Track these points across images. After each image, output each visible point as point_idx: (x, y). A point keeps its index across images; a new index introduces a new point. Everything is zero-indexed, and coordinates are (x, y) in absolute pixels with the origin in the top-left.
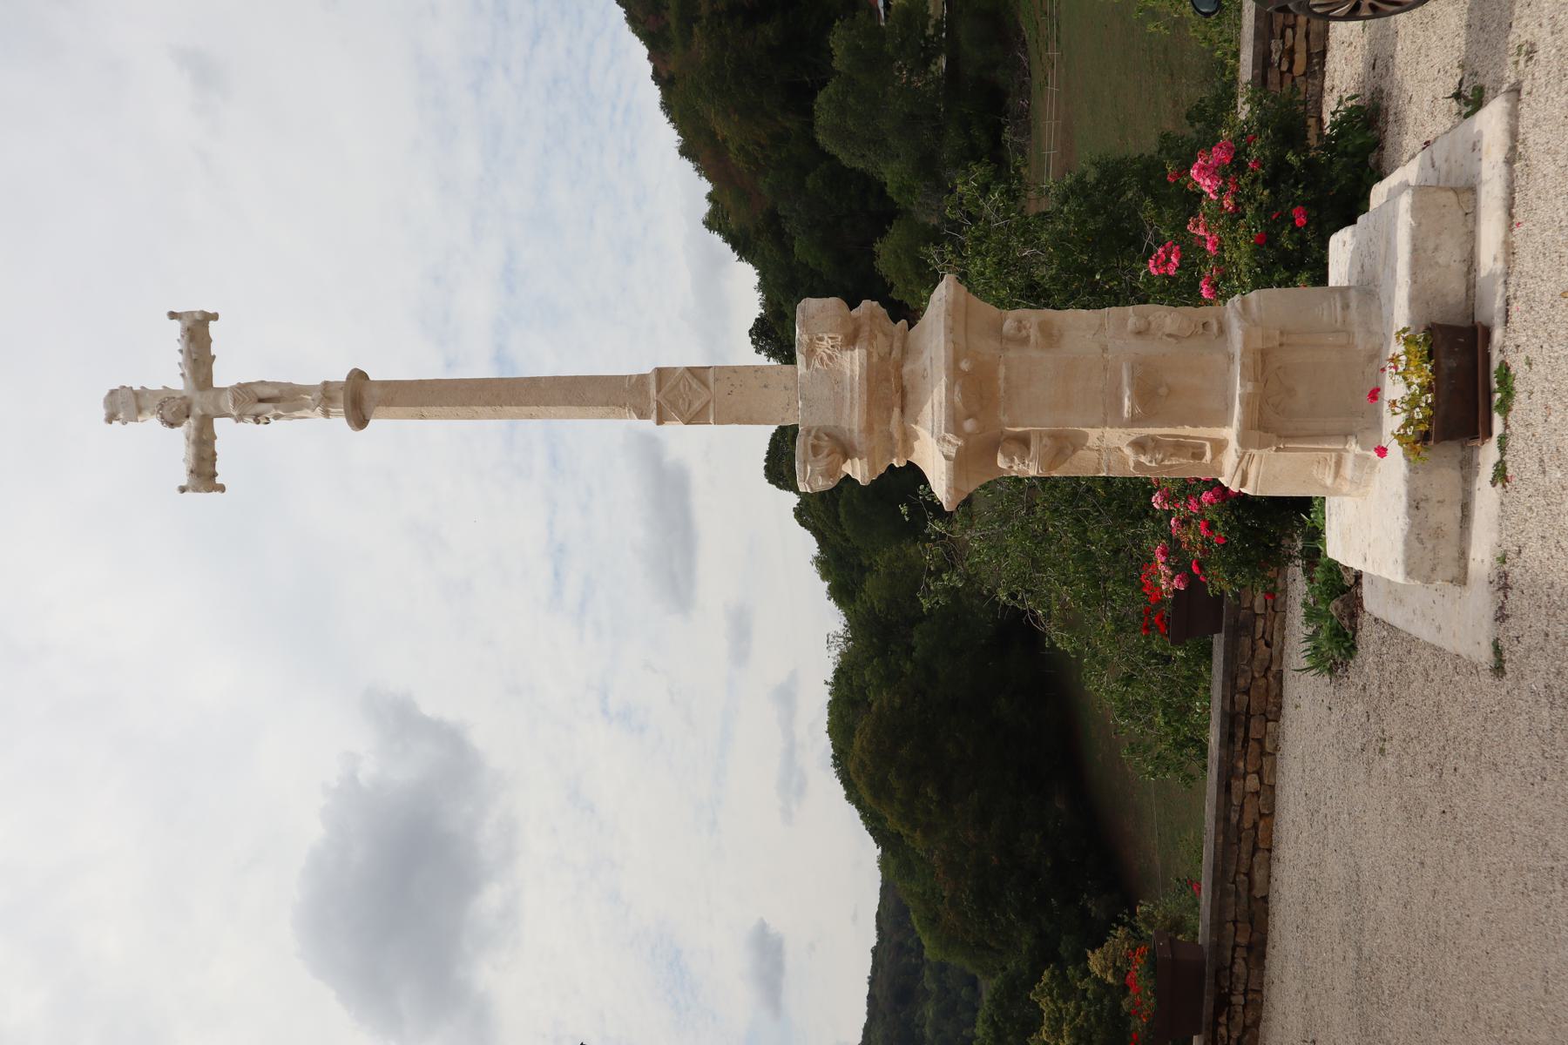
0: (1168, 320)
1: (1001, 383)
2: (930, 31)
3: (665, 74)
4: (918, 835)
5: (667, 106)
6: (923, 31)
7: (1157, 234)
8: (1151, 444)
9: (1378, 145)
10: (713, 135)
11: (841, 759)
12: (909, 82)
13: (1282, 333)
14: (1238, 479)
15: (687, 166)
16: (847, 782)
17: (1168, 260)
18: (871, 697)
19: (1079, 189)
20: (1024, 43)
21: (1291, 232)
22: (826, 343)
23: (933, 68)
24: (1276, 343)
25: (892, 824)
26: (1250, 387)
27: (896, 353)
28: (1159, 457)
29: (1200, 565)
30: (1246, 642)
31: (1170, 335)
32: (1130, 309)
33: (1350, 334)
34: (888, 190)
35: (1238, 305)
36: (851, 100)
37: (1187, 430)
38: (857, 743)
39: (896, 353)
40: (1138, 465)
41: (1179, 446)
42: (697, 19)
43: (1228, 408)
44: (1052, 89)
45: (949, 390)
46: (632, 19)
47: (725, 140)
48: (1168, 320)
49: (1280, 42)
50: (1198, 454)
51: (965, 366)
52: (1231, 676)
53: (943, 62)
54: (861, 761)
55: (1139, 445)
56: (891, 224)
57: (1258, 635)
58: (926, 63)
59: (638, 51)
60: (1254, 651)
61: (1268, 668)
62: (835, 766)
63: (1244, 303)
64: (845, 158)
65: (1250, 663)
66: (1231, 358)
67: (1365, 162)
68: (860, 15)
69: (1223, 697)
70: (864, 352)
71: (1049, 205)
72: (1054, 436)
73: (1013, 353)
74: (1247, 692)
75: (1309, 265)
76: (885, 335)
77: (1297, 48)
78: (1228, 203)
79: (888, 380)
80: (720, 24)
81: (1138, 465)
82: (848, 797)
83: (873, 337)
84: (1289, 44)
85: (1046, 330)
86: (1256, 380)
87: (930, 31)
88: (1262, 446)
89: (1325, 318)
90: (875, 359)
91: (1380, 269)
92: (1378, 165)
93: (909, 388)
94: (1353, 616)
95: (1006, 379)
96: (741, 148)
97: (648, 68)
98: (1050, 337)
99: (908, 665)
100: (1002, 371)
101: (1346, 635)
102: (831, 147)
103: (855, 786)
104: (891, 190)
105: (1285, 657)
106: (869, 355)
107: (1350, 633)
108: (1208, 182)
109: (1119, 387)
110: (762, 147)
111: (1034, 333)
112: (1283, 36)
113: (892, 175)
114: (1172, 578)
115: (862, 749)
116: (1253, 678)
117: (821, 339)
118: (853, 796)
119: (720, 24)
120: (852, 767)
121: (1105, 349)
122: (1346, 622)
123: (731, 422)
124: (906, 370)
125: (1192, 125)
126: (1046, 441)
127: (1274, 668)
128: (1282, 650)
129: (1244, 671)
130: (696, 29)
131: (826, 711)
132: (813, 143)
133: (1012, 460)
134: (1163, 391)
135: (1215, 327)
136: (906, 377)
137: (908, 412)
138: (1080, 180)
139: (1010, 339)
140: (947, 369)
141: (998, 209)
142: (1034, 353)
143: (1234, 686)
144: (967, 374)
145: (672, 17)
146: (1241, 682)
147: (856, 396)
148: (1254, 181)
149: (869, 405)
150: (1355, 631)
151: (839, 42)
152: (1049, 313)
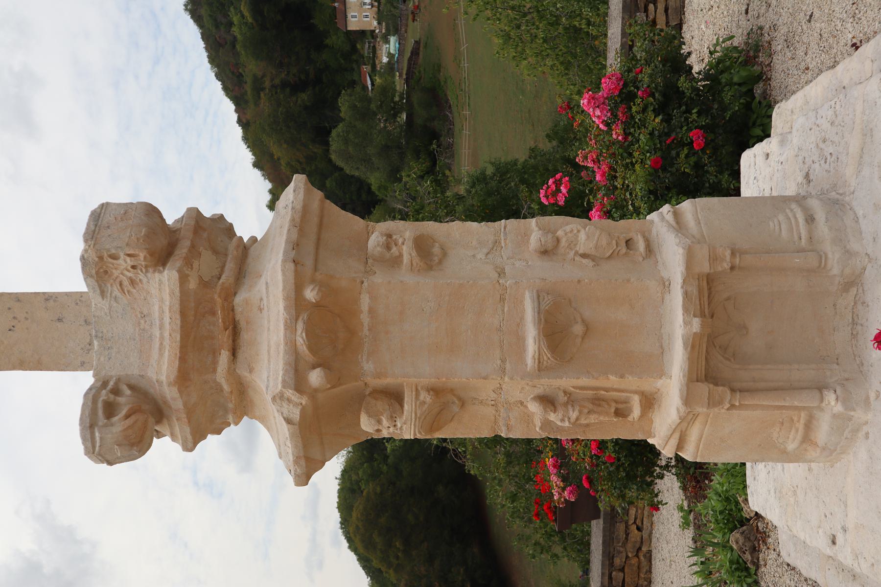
0: (582, 236)
1: (365, 318)
2: (397, 99)
3: (244, 121)
4: (391, 571)
5: (246, 138)
6: (393, 99)
7: (530, 208)
8: (562, 398)
9: (763, 77)
10: (272, 155)
11: (345, 523)
12: (385, 127)
13: (733, 254)
14: (674, 442)
15: (257, 173)
16: (349, 539)
17: (558, 190)
18: (363, 487)
19: (480, 179)
20: (450, 107)
21: (687, 156)
22: (124, 263)
23: (399, 119)
24: (726, 266)
25: (376, 563)
26: (696, 324)
27: (227, 277)
28: (574, 415)
29: (590, 480)
30: (621, 527)
31: (584, 256)
32: (533, 222)
33: (822, 257)
34: (373, 188)
35: (670, 217)
36: (351, 136)
37: (613, 380)
38: (354, 514)
39: (227, 277)
40: (546, 424)
41: (598, 402)
42: (263, 89)
43: (663, 350)
44: (466, 132)
45: (290, 327)
46: (225, 89)
47: (279, 159)
48: (582, 236)
49: (643, 15)
50: (621, 413)
51: (310, 294)
52: (609, 557)
53: (404, 116)
54: (357, 526)
55: (547, 401)
56: (374, 207)
57: (631, 522)
58: (395, 116)
59: (229, 107)
60: (627, 535)
61: (640, 549)
62: (342, 528)
63: (676, 215)
64: (348, 170)
65: (624, 545)
66: (665, 285)
67: (750, 93)
68: (358, 89)
69: (603, 574)
70: (175, 275)
71: (462, 190)
72: (436, 391)
73: (379, 278)
74: (622, 570)
75: (727, 184)
76: (215, 252)
77: (658, 21)
78: (617, 134)
79: (214, 313)
80: (276, 93)
81: (546, 424)
82: (350, 547)
83: (194, 252)
84: (651, 17)
85: (422, 246)
86: (702, 315)
87: (397, 99)
88: (713, 403)
89: (784, 234)
90: (193, 284)
91: (849, 172)
92: (765, 95)
93: (242, 324)
94: (755, 550)
95: (371, 311)
96: (288, 164)
97: (235, 117)
98: (428, 255)
99: (385, 467)
100: (365, 302)
101: (747, 569)
102: (340, 163)
103: (353, 541)
104: (373, 188)
105: (654, 540)
106: (183, 279)
107: (753, 568)
108: (598, 113)
109: (520, 323)
110: (301, 163)
111: (407, 251)
112: (646, 10)
113: (374, 180)
114: (564, 489)
115: (358, 519)
116: (627, 557)
117: (115, 257)
118: (353, 547)
119: (276, 93)
120: (351, 529)
121: (501, 273)
122: (748, 556)
123: (14, 368)
124: (238, 300)
125: (550, 141)
126: (424, 395)
127: (644, 549)
128: (651, 534)
129: (620, 552)
130: (262, 95)
131: (336, 495)
132: (330, 160)
133: (379, 422)
134: (578, 329)
135: (641, 246)
136: (238, 309)
137: (241, 356)
138: (483, 173)
139: (381, 260)
140: (286, 298)
141: (429, 193)
142: (410, 279)
143: (612, 564)
144: (317, 305)
145: (248, 88)
146: (618, 561)
147: (166, 334)
148: (644, 110)
149: (183, 347)
150: (758, 567)
151: (344, 104)
152: (430, 227)
